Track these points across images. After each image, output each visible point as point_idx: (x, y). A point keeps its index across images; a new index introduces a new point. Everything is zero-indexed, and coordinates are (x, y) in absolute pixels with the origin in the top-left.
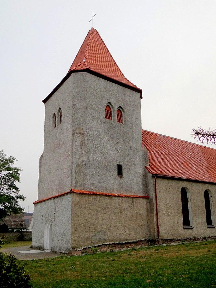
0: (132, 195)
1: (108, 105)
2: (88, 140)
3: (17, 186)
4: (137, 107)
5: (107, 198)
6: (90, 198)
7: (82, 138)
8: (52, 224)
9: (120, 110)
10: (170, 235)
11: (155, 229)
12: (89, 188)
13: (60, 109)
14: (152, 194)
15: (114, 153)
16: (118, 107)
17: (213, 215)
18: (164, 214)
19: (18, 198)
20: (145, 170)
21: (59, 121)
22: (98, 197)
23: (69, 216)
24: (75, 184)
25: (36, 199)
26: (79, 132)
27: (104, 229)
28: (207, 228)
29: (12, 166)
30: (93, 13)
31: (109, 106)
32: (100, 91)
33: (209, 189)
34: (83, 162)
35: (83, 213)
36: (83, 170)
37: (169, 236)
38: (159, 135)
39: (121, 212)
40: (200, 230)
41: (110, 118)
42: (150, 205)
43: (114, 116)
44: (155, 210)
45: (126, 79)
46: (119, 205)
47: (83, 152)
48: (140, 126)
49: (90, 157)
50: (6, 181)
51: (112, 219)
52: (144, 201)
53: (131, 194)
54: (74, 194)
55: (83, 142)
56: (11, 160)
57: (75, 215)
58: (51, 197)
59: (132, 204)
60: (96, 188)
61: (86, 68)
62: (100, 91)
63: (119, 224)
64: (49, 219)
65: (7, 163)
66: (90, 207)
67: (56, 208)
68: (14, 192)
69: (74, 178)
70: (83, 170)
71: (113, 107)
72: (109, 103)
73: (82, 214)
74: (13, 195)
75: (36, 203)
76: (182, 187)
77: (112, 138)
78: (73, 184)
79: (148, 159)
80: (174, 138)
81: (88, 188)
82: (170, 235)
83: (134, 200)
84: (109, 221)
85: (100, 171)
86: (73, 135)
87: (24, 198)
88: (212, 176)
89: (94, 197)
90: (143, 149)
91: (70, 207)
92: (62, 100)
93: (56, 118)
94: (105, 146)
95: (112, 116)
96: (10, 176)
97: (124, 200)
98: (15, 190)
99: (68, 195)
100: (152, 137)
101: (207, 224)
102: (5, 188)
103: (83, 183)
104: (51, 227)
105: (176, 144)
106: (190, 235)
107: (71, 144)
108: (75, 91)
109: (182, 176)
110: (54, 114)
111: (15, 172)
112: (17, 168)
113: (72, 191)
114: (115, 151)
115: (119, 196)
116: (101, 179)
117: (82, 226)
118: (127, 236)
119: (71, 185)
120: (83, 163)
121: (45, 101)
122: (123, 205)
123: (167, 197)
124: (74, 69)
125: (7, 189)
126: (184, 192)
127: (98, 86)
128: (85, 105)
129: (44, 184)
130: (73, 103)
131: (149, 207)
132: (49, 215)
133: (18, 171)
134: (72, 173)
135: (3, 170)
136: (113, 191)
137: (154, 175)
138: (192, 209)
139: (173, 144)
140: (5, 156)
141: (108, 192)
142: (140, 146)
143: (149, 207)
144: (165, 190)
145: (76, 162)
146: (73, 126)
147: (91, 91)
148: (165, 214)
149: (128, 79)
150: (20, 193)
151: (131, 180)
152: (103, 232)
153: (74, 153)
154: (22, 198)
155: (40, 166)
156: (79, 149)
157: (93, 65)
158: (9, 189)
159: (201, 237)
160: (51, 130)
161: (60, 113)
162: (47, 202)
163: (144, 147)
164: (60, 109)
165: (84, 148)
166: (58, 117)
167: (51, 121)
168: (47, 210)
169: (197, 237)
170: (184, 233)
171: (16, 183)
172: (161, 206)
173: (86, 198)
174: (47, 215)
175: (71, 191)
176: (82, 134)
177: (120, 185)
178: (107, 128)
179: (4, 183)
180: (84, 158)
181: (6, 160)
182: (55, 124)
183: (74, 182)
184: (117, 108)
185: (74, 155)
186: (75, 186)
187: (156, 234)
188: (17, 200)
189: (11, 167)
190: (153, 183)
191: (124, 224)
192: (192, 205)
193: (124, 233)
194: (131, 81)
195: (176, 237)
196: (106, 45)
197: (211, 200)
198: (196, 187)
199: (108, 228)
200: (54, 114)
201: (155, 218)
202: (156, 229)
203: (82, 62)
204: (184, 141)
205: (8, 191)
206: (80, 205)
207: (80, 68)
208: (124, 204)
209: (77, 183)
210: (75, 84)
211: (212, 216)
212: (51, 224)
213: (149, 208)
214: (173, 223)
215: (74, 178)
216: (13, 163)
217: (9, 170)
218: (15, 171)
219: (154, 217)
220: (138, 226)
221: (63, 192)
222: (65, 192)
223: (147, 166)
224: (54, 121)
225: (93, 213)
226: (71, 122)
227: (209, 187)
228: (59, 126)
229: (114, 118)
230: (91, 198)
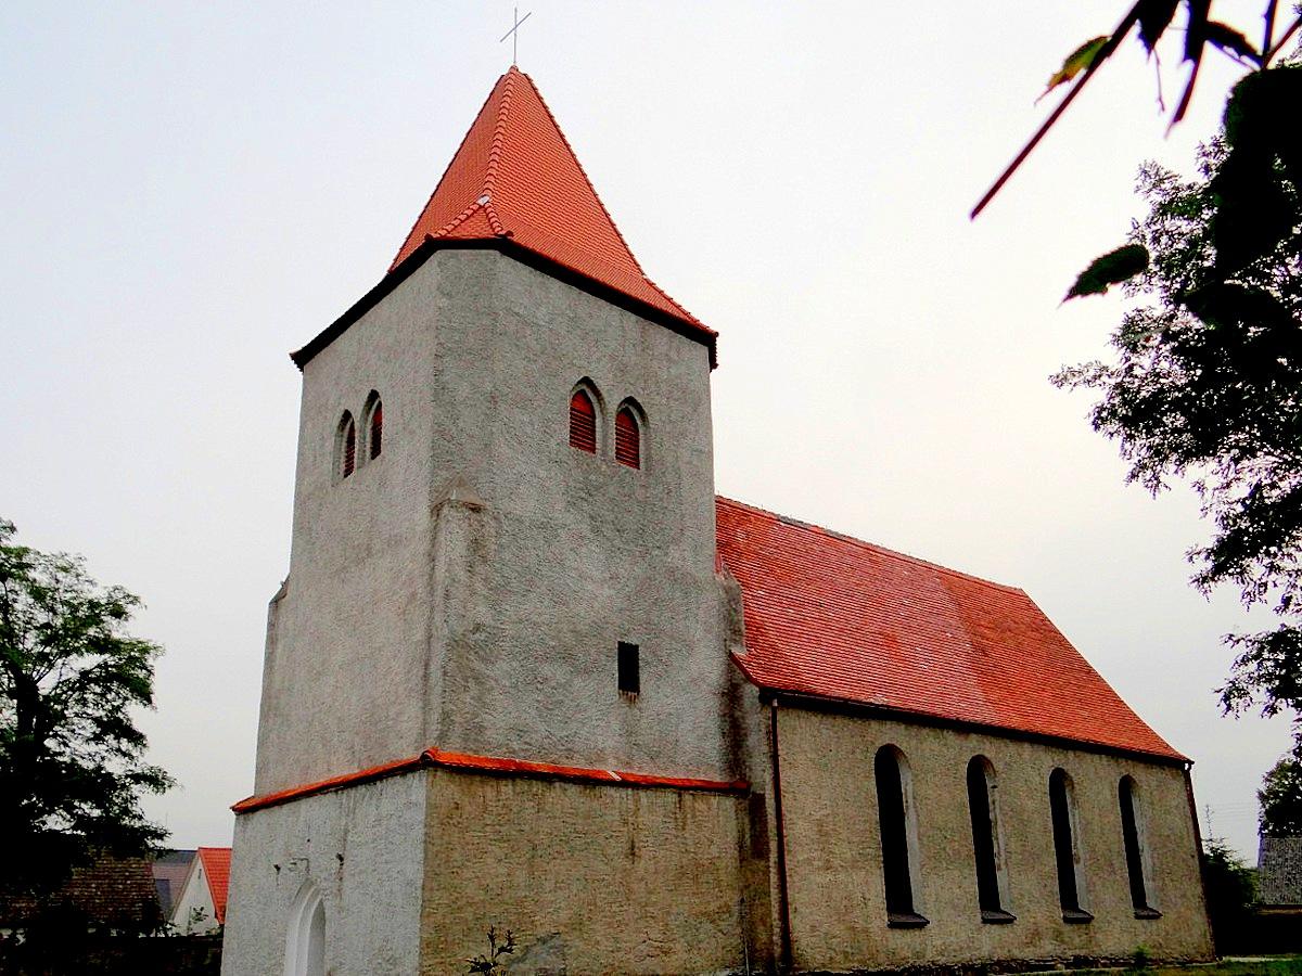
0: (675, 777)
1: (583, 392)
2: (498, 535)
3: (137, 726)
4: (698, 403)
5: (573, 790)
6: (503, 789)
7: (476, 525)
8: (327, 904)
9: (631, 414)
10: (834, 955)
11: (772, 926)
12: (499, 746)
13: (374, 395)
14: (761, 775)
15: (607, 592)
16: (623, 398)
17: (1003, 867)
18: (809, 861)
19: (137, 782)
20: (730, 671)
21: (368, 446)
22: (537, 787)
23: (414, 870)
24: (440, 726)
25: (246, 790)
26: (459, 499)
27: (562, 929)
28: (981, 925)
29: (118, 630)
30: (516, 10)
31: (585, 397)
32: (551, 330)
33: (987, 755)
34: (478, 628)
35: (475, 856)
36: (478, 665)
37: (831, 958)
38: (779, 519)
39: (632, 852)
40: (953, 933)
41: (588, 443)
42: (753, 823)
43: (605, 437)
44: (773, 845)
45: (651, 285)
46: (626, 823)
47: (479, 586)
48: (712, 489)
49: (507, 607)
50: (85, 699)
51: (597, 883)
52: (729, 803)
53: (676, 772)
54: (439, 773)
55: (476, 545)
56: (115, 604)
57: (439, 865)
58: (322, 780)
59: (676, 818)
60: (526, 743)
61: (496, 235)
62: (551, 330)
63: (625, 907)
64: (308, 883)
65: (95, 619)
66: (502, 829)
67: (346, 832)
68: (124, 754)
69: (436, 701)
70: (478, 665)
71: (602, 399)
72: (586, 381)
73: (468, 861)
74: (116, 767)
75: (244, 810)
76: (879, 744)
77: (596, 531)
78: (434, 728)
79: (738, 625)
80: (836, 533)
81: (498, 744)
82: (834, 955)
83: (687, 798)
84: (582, 895)
85: (546, 670)
86: (436, 510)
87: (166, 782)
88: (994, 697)
89: (522, 785)
90: (720, 578)
91: (420, 831)
92: (390, 360)
93: (357, 435)
94: (568, 563)
95: (598, 436)
96: (106, 677)
97: (644, 801)
98: (125, 744)
99: (410, 775)
100: (750, 527)
101: (983, 908)
102: (81, 732)
103: (476, 720)
104: (320, 918)
105: (849, 560)
106: (918, 955)
107: (424, 546)
108: (445, 324)
109: (880, 699)
110: (347, 415)
111: (131, 659)
112: (140, 642)
113: (429, 757)
114: (609, 587)
115: (624, 784)
116: (550, 707)
117: (468, 914)
118: (658, 959)
119: (424, 733)
120: (477, 635)
121: (302, 358)
122: (640, 819)
123: (821, 781)
124: (443, 233)
125: (91, 739)
126: (888, 764)
127: (543, 309)
128: (489, 387)
129: (288, 720)
130: (438, 373)
131: (747, 830)
132: (312, 865)
133: (147, 656)
134: (426, 677)
135: (77, 650)
136: (601, 756)
137: (767, 695)
138: (919, 839)
139: (834, 559)
140: (91, 587)
141: (578, 764)
142: (711, 565)
143: (747, 830)
144: (814, 756)
145: (446, 632)
146: (433, 474)
147: (512, 328)
148: (816, 863)
149: (660, 286)
150: (146, 760)
151: (672, 711)
152: (556, 942)
153: (440, 592)
154: (155, 780)
155: (272, 641)
156: (462, 575)
157: (512, 217)
158: (97, 738)
159: (959, 962)
160: (329, 484)
161: (372, 412)
162: (304, 806)
163: (726, 570)
164: (374, 395)
165: (479, 568)
166: (362, 431)
167: (331, 444)
168: (300, 841)
169: (942, 960)
170: (892, 945)
171: (135, 713)
172: (799, 829)
173: (488, 790)
174: (302, 866)
175: (424, 757)
176: (476, 509)
177: (629, 732)
178: (578, 485)
179: (77, 709)
180: (482, 613)
181: (93, 605)
182: (350, 458)
183: (435, 716)
184: (620, 406)
185: (439, 599)
186: (442, 737)
187: (778, 951)
188: (135, 789)
189: (116, 635)
190: (763, 727)
191: (646, 905)
192: (919, 825)
193: (642, 947)
194: (654, 281)
195: (859, 961)
196: (568, 139)
197: (994, 803)
198: (936, 747)
199: (577, 925)
200: (347, 415)
201: (774, 878)
202: (777, 930)
203: (475, 207)
204: (878, 546)
205: (92, 747)
206: (460, 820)
207: (467, 232)
208: (645, 818)
209: (452, 721)
210: (449, 295)
211: (1000, 869)
212: (321, 903)
213: (747, 836)
214: (844, 903)
215: (436, 701)
216: (126, 620)
217: (102, 652)
218: (132, 654)
219: (771, 875)
220: (703, 914)
221: (383, 761)
222: (394, 759)
223: (740, 652)
224: (344, 444)
225: (514, 855)
226: (425, 454)
227: (989, 749)
228: (368, 472)
229: (605, 445)
230: (507, 789)
